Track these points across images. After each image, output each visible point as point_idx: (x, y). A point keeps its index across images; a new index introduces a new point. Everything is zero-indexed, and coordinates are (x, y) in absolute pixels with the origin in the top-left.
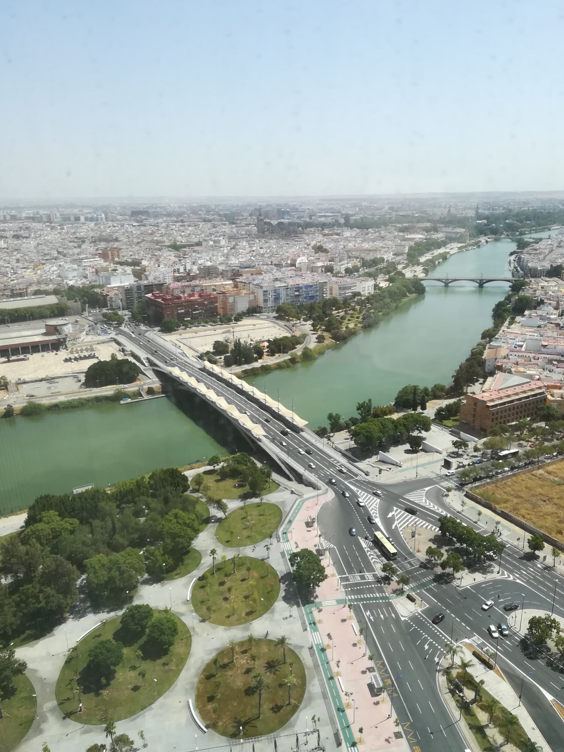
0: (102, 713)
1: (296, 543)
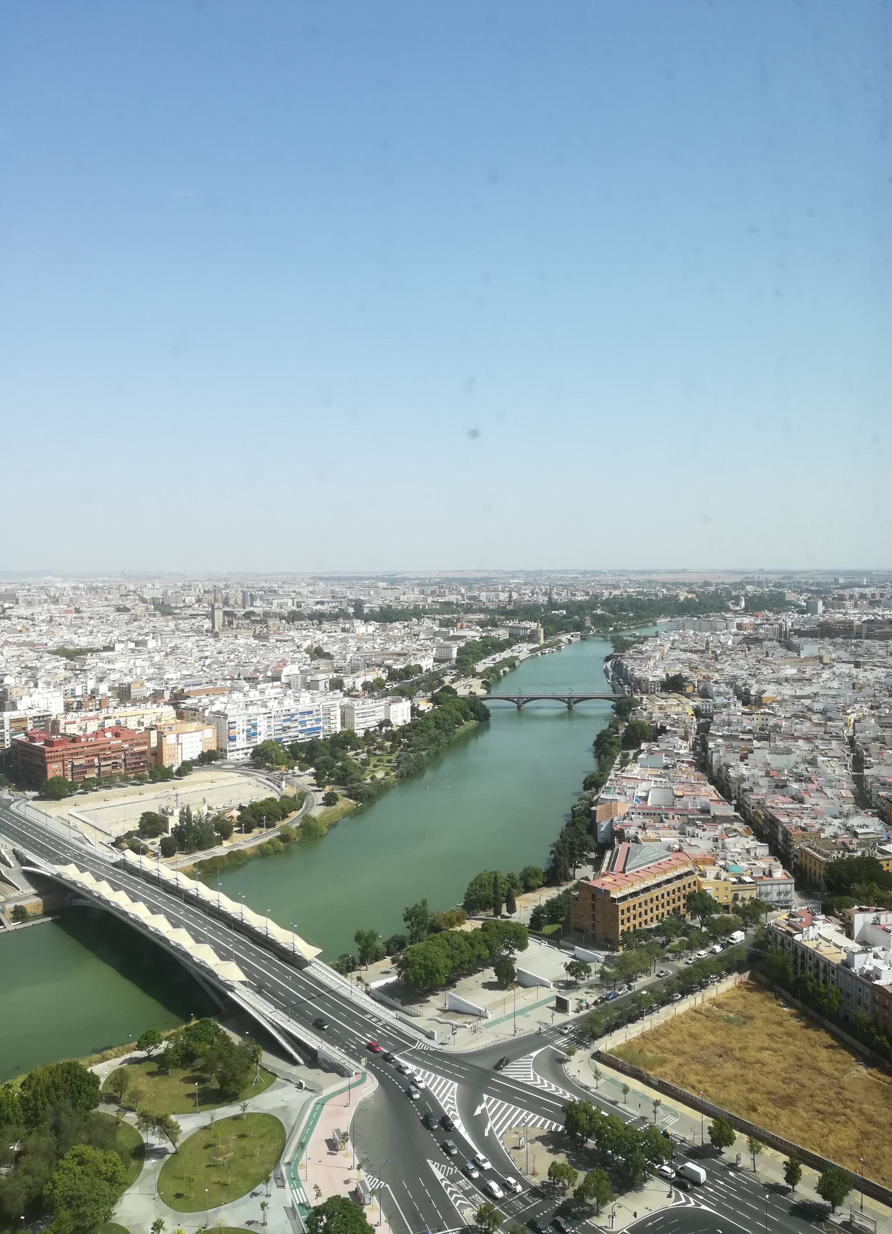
0: (516, 980)
1: (316, 1187)
